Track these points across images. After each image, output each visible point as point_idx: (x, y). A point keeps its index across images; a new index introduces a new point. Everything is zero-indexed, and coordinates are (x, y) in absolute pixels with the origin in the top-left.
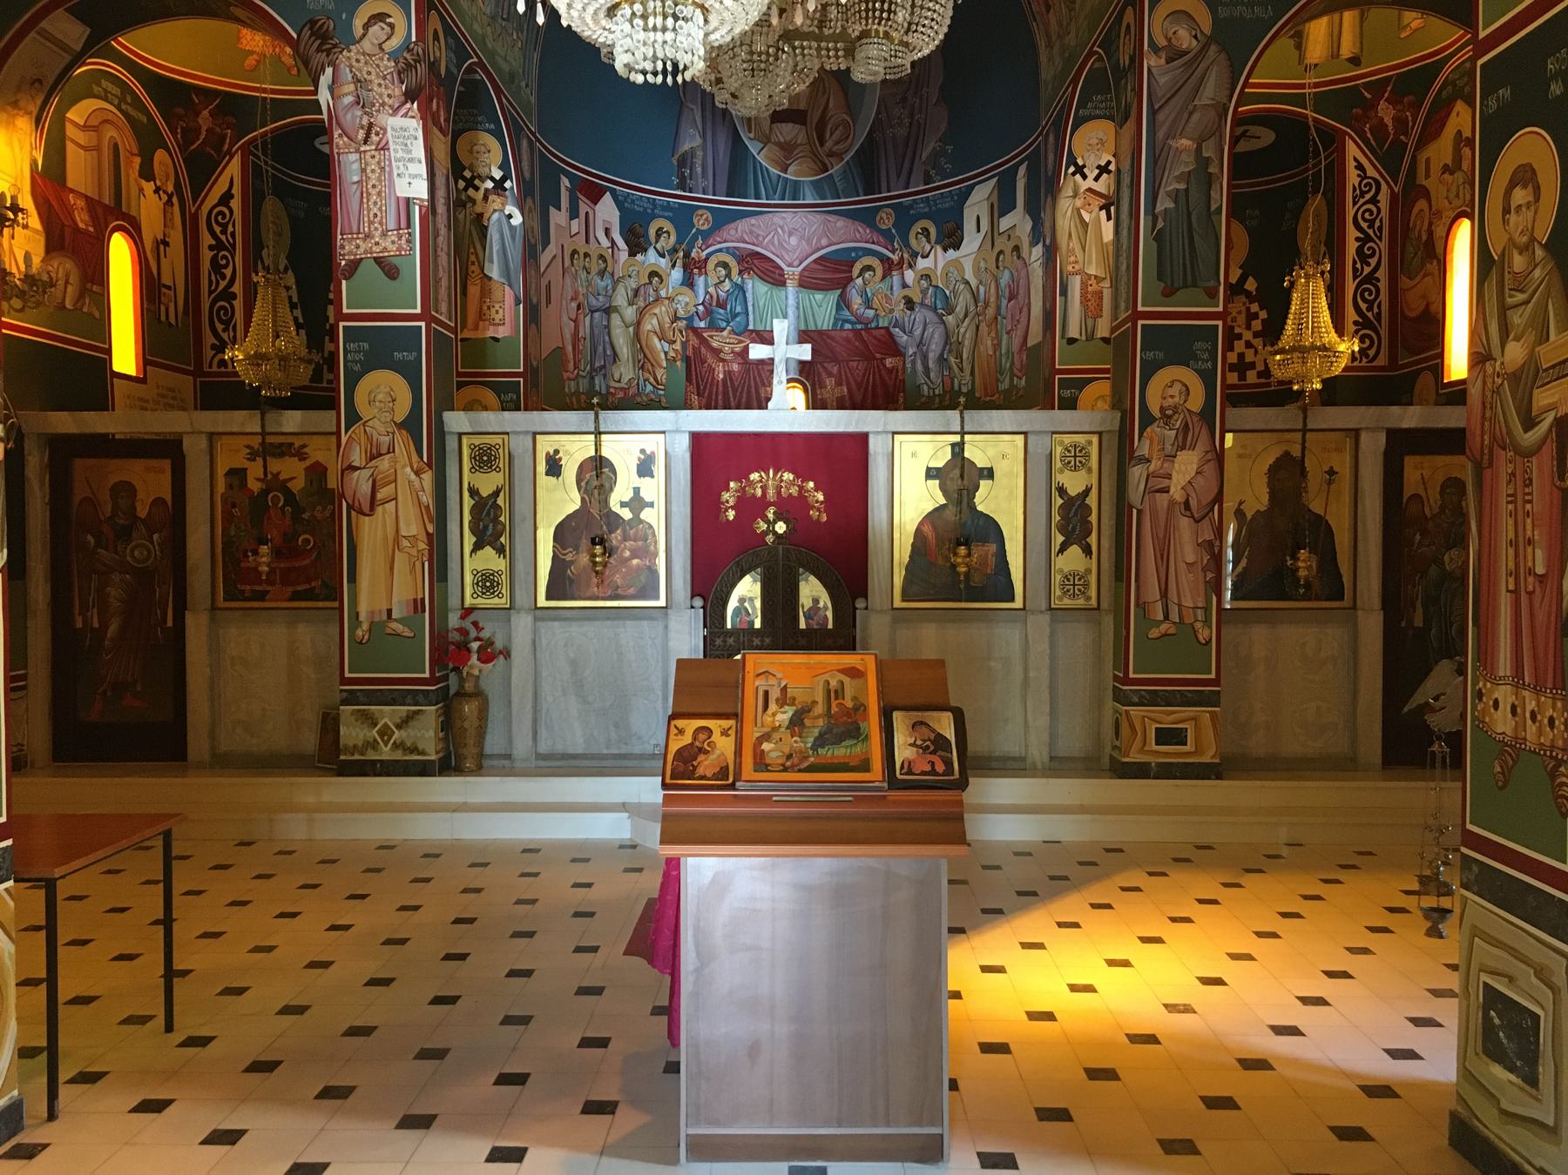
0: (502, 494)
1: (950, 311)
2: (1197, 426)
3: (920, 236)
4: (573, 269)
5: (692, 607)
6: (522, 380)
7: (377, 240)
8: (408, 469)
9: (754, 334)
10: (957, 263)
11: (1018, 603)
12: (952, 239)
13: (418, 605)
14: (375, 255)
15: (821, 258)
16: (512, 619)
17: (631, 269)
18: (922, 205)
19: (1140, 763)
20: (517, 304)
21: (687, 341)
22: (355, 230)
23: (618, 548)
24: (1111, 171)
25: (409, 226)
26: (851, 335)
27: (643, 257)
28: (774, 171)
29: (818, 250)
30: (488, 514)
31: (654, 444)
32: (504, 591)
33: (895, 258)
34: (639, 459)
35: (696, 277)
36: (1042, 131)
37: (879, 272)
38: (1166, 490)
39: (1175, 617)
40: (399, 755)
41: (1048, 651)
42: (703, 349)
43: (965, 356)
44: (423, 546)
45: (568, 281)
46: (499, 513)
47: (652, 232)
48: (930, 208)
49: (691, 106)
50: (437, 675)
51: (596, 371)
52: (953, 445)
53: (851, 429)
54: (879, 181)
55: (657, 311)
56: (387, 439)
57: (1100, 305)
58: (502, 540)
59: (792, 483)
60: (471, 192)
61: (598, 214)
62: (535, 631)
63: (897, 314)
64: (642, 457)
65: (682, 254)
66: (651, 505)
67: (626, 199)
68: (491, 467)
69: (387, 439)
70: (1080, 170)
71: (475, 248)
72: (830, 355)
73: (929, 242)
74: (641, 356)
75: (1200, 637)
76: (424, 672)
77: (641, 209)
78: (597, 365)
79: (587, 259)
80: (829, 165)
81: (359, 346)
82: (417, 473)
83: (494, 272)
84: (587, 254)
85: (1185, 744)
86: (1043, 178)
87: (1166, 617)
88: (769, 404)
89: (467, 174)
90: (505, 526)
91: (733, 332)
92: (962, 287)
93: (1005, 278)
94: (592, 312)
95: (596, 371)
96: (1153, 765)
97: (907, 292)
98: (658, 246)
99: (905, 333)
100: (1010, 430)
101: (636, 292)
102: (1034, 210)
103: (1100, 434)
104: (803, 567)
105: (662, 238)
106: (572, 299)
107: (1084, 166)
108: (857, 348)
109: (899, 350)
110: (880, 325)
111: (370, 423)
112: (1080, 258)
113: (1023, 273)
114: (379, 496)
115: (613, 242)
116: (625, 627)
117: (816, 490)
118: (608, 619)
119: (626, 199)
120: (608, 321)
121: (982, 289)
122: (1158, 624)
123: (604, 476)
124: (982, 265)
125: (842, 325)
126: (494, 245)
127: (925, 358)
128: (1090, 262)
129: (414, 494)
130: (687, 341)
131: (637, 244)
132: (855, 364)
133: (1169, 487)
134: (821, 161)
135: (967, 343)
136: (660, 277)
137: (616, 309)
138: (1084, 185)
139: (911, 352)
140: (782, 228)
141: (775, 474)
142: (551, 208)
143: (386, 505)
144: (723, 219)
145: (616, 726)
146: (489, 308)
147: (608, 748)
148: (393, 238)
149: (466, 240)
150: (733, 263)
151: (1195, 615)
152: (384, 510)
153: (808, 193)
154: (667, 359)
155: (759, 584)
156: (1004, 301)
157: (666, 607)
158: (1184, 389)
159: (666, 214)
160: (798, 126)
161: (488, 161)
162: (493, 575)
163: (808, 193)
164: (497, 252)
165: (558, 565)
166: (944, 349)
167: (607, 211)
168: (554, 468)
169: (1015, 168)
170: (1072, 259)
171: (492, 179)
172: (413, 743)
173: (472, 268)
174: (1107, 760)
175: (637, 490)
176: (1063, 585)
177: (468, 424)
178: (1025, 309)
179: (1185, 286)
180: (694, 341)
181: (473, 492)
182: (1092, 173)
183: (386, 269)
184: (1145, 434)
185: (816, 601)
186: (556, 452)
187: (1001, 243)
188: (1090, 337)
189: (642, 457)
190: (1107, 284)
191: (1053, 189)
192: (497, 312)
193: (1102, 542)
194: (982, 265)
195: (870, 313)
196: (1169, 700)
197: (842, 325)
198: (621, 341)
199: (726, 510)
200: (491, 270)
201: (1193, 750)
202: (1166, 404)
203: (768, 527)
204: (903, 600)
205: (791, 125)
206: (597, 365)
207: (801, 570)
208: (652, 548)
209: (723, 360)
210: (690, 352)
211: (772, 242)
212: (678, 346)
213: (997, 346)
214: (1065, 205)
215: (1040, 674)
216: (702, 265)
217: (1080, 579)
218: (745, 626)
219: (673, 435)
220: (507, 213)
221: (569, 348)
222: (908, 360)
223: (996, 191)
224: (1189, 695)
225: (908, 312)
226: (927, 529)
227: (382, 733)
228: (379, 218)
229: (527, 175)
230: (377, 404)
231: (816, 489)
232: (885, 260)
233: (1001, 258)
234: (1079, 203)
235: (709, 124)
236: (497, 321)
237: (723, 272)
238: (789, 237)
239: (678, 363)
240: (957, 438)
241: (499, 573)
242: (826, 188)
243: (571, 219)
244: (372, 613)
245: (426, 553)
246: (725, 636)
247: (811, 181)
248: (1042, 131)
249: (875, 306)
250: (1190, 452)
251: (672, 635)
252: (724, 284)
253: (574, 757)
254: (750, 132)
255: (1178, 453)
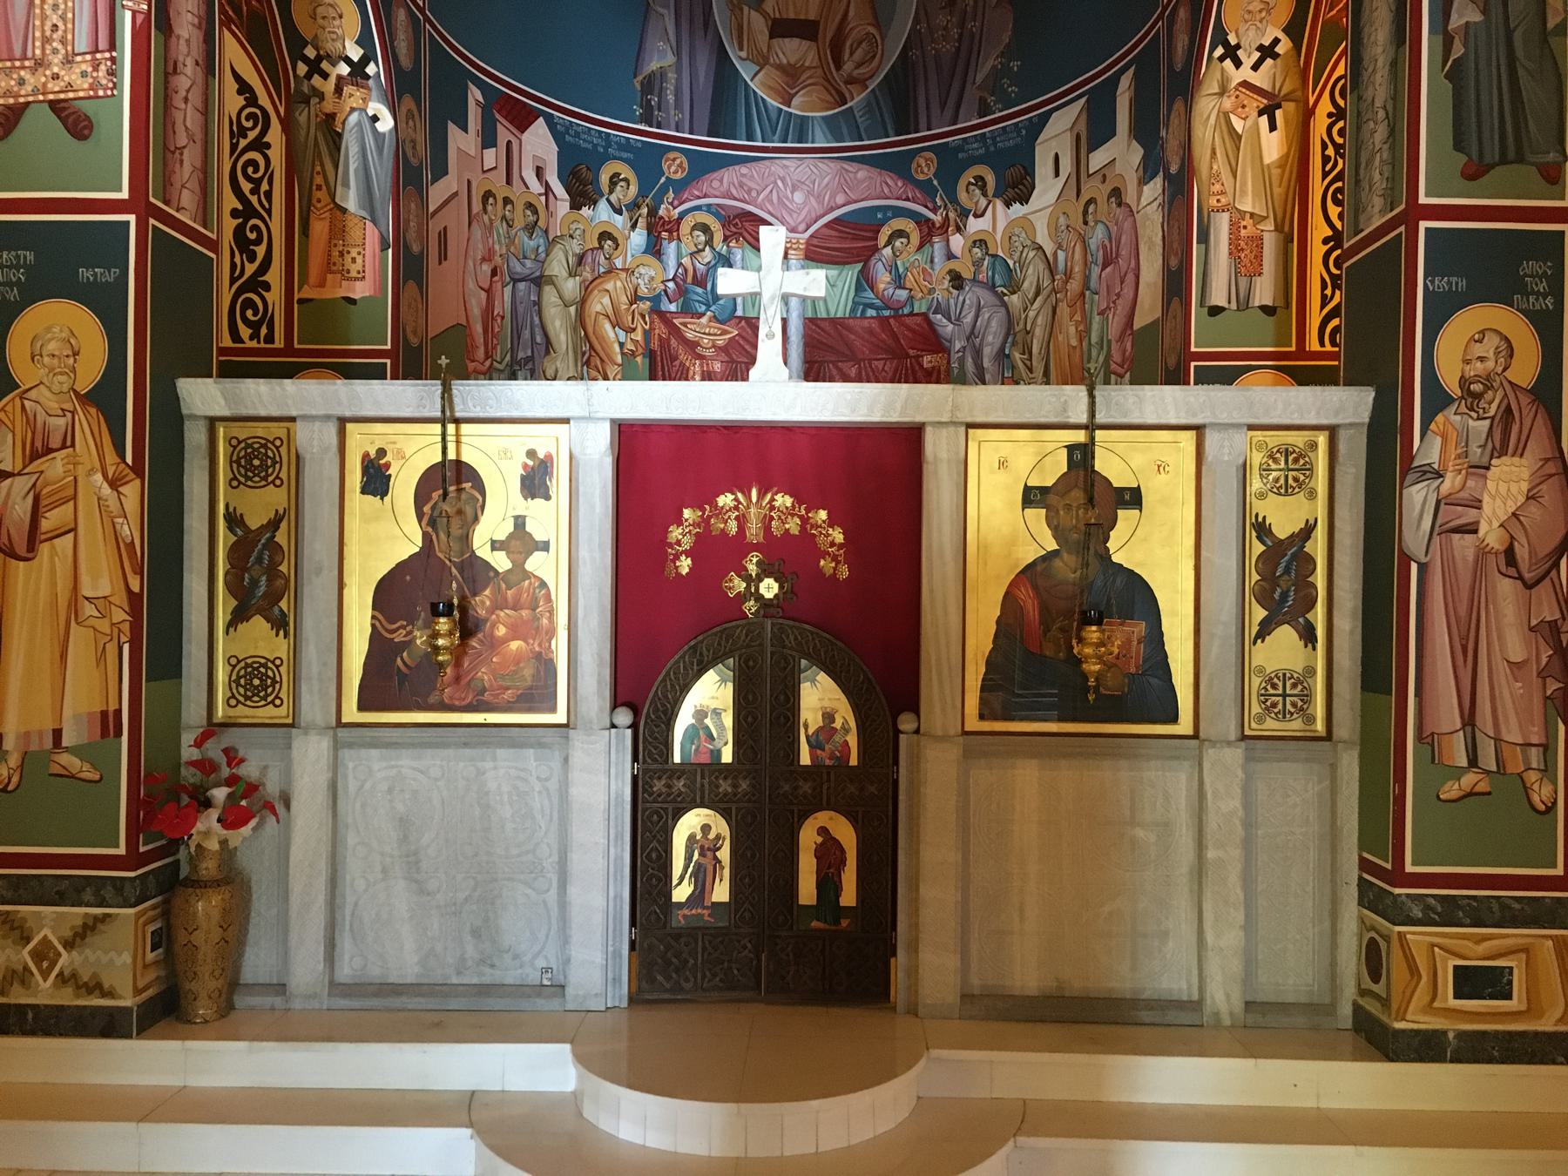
0: (284, 525)
1: (1014, 288)
2: (1528, 413)
3: (972, 187)
4: (486, 218)
5: (613, 726)
6: (388, 361)
7: (56, 70)
8: (98, 477)
9: (743, 323)
10: (1026, 223)
11: (1185, 725)
12: (1018, 188)
13: (108, 724)
14: (51, 97)
15: (836, 221)
16: (295, 744)
17: (573, 226)
18: (975, 146)
19: (1427, 1031)
20: (384, 248)
21: (652, 329)
22: (18, 52)
23: (486, 620)
24: (1278, 55)
25: (112, 46)
26: (875, 325)
27: (590, 212)
28: (773, 103)
29: (832, 209)
30: (259, 560)
31: (544, 440)
32: (283, 695)
33: (937, 218)
34: (525, 466)
35: (665, 243)
36: (1163, 13)
37: (915, 238)
38: (1472, 529)
39: (1488, 760)
40: (67, 998)
41: (1241, 813)
42: (673, 341)
43: (1035, 350)
44: (120, 615)
45: (477, 232)
46: (278, 558)
47: (604, 178)
48: (987, 148)
49: (661, 10)
50: (142, 849)
51: (519, 363)
52: (1071, 449)
53: (894, 417)
54: (916, 98)
55: (609, 286)
56: (61, 422)
57: (1259, 257)
58: (283, 604)
59: (791, 512)
60: (317, 80)
61: (526, 148)
62: (335, 766)
63: (939, 295)
64: (530, 463)
65: (645, 211)
66: (545, 547)
67: (567, 129)
68: (265, 478)
69: (61, 422)
70: (1232, 53)
71: (322, 165)
72: (848, 352)
73: (985, 195)
74: (586, 348)
75: (1536, 799)
76: (117, 846)
77: (590, 146)
78: (521, 355)
79: (509, 207)
80: (847, 95)
81: (18, 257)
82: (115, 484)
83: (351, 201)
84: (507, 201)
85: (1509, 997)
86: (1164, 72)
87: (1473, 762)
88: (752, 373)
89: (310, 52)
90: (287, 580)
91: (715, 318)
92: (1032, 254)
93: (1098, 236)
94: (515, 281)
95: (519, 363)
96: (1451, 1035)
97: (953, 265)
98: (613, 198)
99: (949, 319)
100: (1173, 421)
101: (581, 259)
102: (1146, 131)
103: (1332, 431)
104: (808, 656)
105: (618, 188)
106: (483, 260)
107: (1238, 46)
108: (883, 341)
109: (940, 344)
110: (916, 311)
111: (33, 394)
112: (1229, 190)
113: (1127, 225)
114: (45, 525)
115: (548, 187)
116: (494, 759)
117: (831, 525)
118: (466, 745)
119: (567, 129)
120: (539, 295)
121: (1061, 255)
122: (1458, 773)
123: (464, 496)
124: (1062, 220)
125: (863, 311)
126: (351, 161)
127: (978, 354)
128: (1244, 193)
129: (109, 529)
130: (652, 329)
131: (582, 193)
132: (880, 364)
133: (1477, 523)
134: (836, 90)
135: (1038, 332)
136: (615, 240)
137: (551, 281)
138: (1237, 76)
139: (958, 346)
140: (783, 179)
141: (761, 496)
142: (450, 124)
143: (56, 541)
144: (702, 166)
145: (476, 933)
146: (341, 254)
147: (459, 973)
148: (84, 67)
149: (310, 152)
150: (715, 225)
151: (1527, 760)
152: (53, 547)
153: (818, 133)
154: (623, 354)
155: (730, 686)
156: (1096, 270)
157: (566, 726)
158: (1504, 346)
159: (625, 155)
160: (808, 43)
161: (339, 32)
162: (265, 666)
163: (818, 133)
164: (356, 170)
165: (381, 650)
166: (1005, 342)
167: (539, 143)
168: (376, 479)
169: (1114, 82)
170: (1217, 187)
171: (348, 61)
172: (95, 975)
173: (319, 194)
174: (1346, 1010)
175: (520, 522)
176: (1264, 696)
177: (222, 402)
178: (1130, 277)
179: (1504, 161)
180: (661, 330)
181: (234, 520)
182: (1248, 58)
183: (71, 120)
184: (1433, 426)
185: (829, 717)
186: (382, 452)
187: (1090, 189)
188: (1244, 305)
189: (530, 463)
190: (1269, 225)
191: (1185, 86)
192: (354, 260)
193: (1336, 621)
194: (1062, 220)
195: (902, 294)
196: (1478, 915)
197: (863, 311)
198: (558, 323)
199: (677, 557)
200: (345, 198)
201: (1523, 1007)
202: (1470, 371)
203: (748, 587)
204: (982, 717)
205: (796, 41)
206: (521, 355)
207: (804, 662)
208: (545, 621)
209: (701, 357)
210: (655, 345)
211: (769, 198)
212: (638, 336)
213: (1084, 334)
214: (1207, 107)
215: (1225, 854)
216: (673, 227)
217: (1294, 686)
218: (705, 759)
219: (583, 425)
220: (371, 113)
221: (478, 328)
222: (954, 357)
223: (1084, 116)
224: (1517, 906)
225: (955, 292)
226: (1025, 595)
227: (38, 956)
228: (60, 33)
229: (406, 62)
230: (46, 360)
231: (831, 522)
232: (921, 221)
233: (1091, 208)
234: (1228, 103)
235: (685, 25)
236: (353, 274)
237: (702, 238)
238: (792, 193)
239: (639, 359)
240: (1080, 436)
241: (276, 663)
242: (842, 121)
243: (484, 146)
244: (27, 735)
245: (126, 627)
246: (670, 778)
247: (823, 118)
248: (1163, 13)
249: (908, 285)
250: (1516, 460)
251: (575, 775)
252: (704, 254)
253: (397, 990)
254: (741, 49)
255: (1494, 462)
